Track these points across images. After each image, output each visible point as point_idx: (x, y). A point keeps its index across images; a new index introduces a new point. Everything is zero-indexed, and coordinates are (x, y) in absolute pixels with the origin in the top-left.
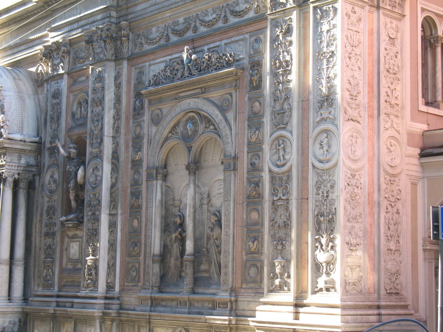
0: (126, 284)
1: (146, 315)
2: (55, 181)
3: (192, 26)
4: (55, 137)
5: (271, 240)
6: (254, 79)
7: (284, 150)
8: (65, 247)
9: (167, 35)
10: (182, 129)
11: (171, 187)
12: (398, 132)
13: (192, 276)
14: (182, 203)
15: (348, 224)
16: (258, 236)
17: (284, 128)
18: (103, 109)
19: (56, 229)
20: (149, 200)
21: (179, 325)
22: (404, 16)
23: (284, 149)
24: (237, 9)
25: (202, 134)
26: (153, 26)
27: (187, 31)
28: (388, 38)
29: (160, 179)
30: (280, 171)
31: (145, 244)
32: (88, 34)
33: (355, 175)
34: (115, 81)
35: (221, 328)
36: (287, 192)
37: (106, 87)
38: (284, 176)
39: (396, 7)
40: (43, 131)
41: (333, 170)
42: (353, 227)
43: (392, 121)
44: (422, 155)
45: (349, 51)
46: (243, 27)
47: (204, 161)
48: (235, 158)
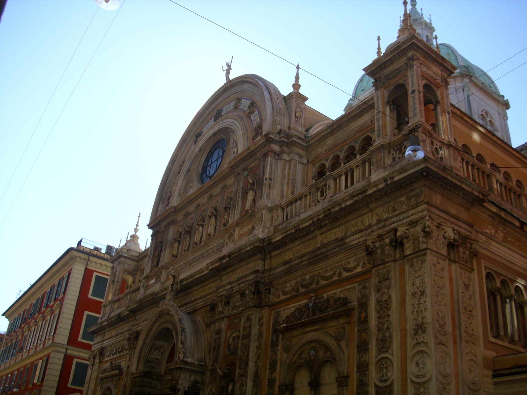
3: (316, 280)
9: (297, 288)
12: (476, 356)
17: (386, 352)
18: (249, 341)
22: (474, 270)
23: (386, 368)
24: (349, 266)
28: (464, 285)
33: (446, 389)
37: (253, 326)
39: (467, 263)
41: (427, 384)
43: (471, 348)
44: (494, 376)
48: (347, 377)
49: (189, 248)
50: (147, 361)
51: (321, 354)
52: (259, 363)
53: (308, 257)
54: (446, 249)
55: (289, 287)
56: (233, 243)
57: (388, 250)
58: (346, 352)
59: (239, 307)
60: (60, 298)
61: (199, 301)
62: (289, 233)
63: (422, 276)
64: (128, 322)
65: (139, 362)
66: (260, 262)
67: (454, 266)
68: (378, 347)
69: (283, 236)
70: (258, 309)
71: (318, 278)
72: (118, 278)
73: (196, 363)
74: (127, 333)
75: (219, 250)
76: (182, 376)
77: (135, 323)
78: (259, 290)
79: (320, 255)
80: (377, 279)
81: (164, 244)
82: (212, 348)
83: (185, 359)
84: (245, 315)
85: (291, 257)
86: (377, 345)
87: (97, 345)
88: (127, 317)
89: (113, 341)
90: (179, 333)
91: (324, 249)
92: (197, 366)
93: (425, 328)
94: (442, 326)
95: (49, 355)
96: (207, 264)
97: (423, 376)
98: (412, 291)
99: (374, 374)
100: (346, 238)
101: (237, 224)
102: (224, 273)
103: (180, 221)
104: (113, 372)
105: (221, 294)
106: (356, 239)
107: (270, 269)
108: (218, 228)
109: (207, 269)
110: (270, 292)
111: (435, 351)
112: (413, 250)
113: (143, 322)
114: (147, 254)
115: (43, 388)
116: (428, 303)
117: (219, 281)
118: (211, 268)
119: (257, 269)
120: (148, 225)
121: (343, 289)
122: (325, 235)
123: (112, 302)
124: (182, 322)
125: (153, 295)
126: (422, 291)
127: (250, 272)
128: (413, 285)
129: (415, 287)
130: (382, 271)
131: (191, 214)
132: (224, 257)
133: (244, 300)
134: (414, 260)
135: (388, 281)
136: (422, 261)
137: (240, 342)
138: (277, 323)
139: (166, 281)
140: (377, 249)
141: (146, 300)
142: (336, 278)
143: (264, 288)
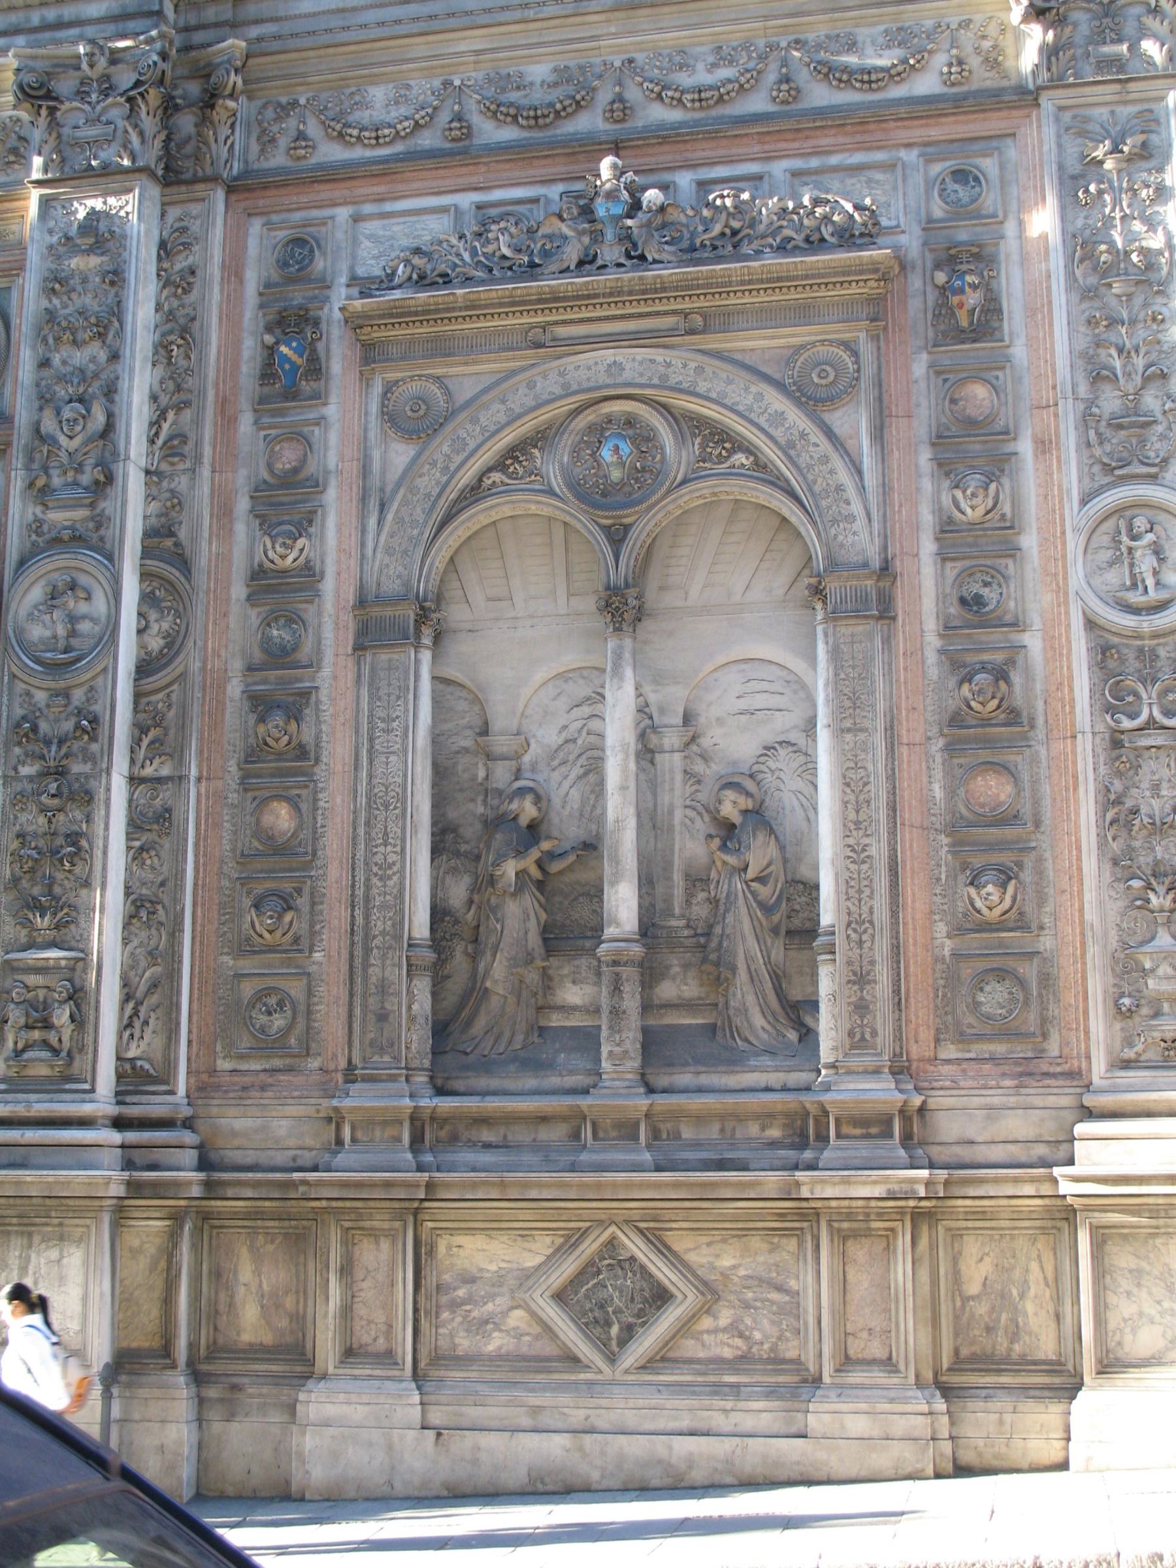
0: (224, 1065)
1: (417, 1186)
5: (1113, 874)
6: (961, 305)
7: (1156, 553)
10: (565, 459)
11: (468, 683)
14: (533, 745)
16: (1020, 865)
17: (1153, 478)
18: (115, 357)
20: (381, 725)
21: (603, 1217)
25: (684, 482)
26: (374, 80)
27: (575, 112)
29: (427, 648)
30: (1145, 624)
32: (31, 63)
34: (159, 259)
35: (868, 1215)
38: (1165, 645)
46: (892, 124)
47: (662, 588)
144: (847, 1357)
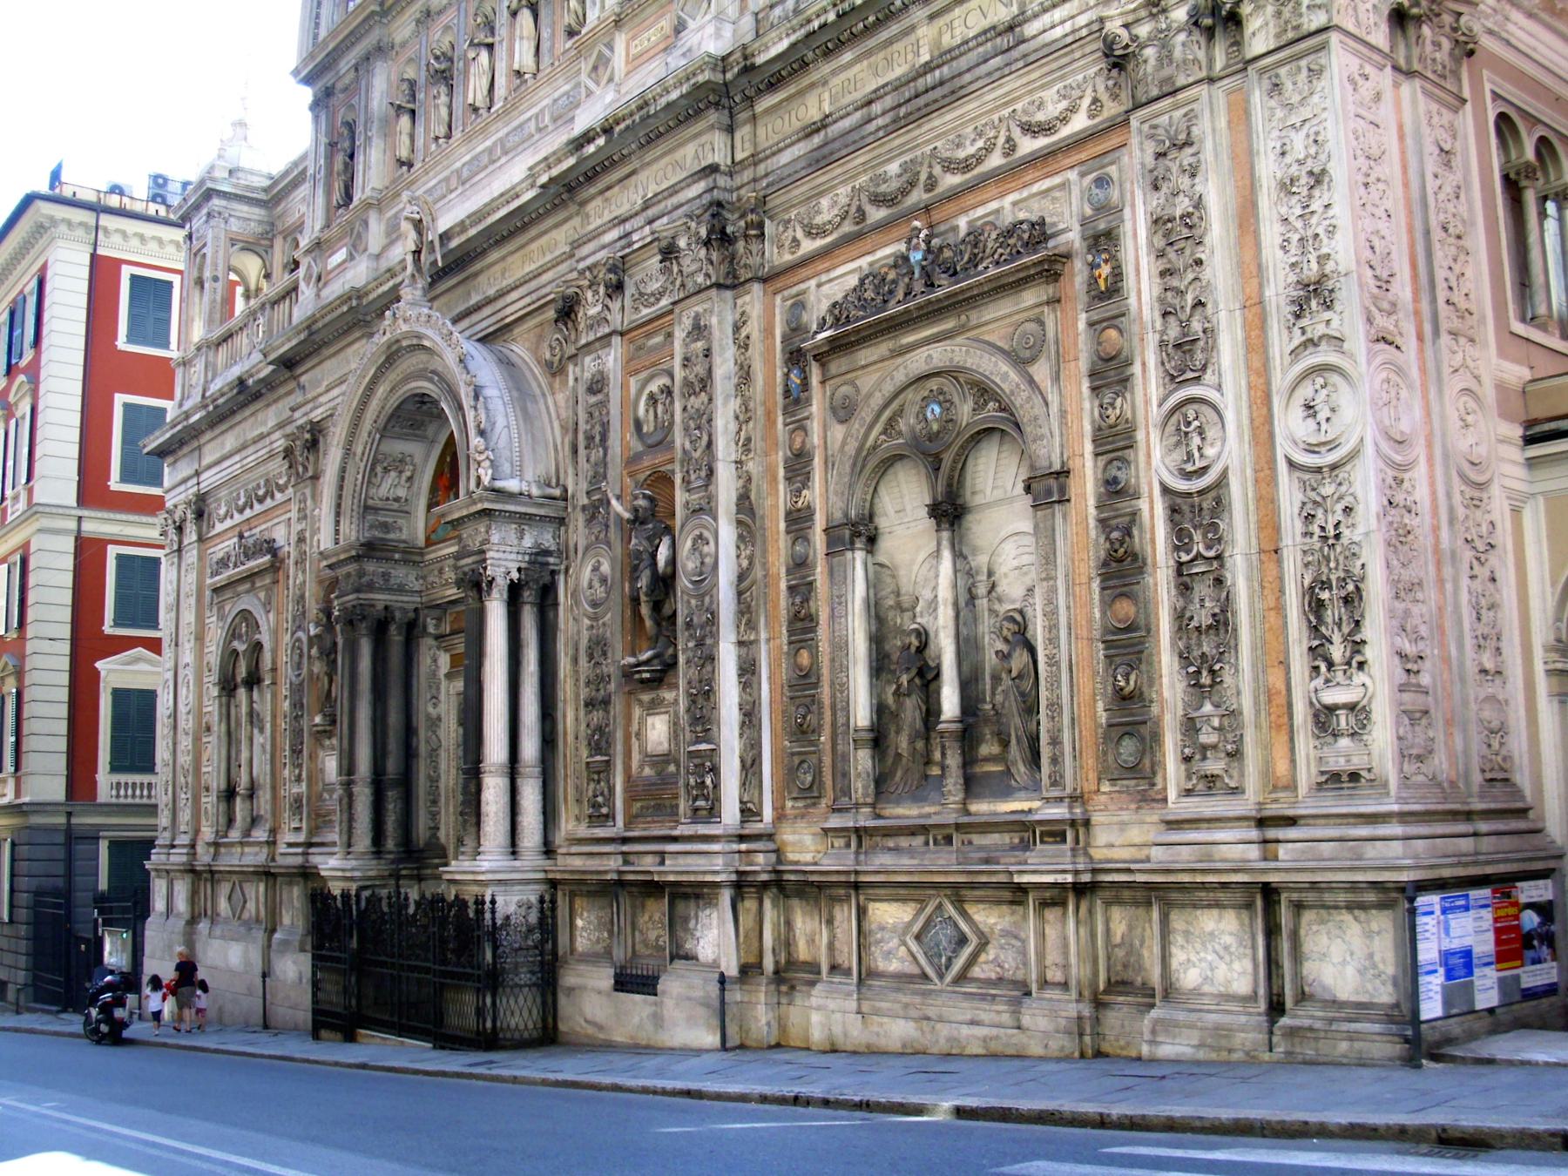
2: (603, 580)
3: (923, 177)
4: (599, 475)
8: (635, 727)
9: (860, 209)
12: (1477, 378)
13: (960, 772)
15: (1397, 604)
18: (710, 400)
19: (612, 687)
22: (1464, 101)
23: (1201, 431)
24: (1040, 117)
28: (1437, 151)
31: (833, 707)
36: (1215, 537)
40: (570, 471)
41: (1348, 467)
42: (1407, 613)
44: (1529, 440)
45: (1364, 169)
47: (974, 493)
48: (1064, 473)
49: (450, 127)
50: (367, 508)
51: (965, 411)
52: (750, 466)
53: (889, 101)
54: (1384, 27)
55: (826, 211)
56: (612, 86)
57: (1184, 44)
58: (1053, 398)
59: (659, 295)
60: (23, 363)
61: (514, 295)
62: (816, 24)
63: (1315, 121)
64: (275, 401)
65: (338, 514)
66: (719, 139)
67: (1408, 89)
68: (1168, 366)
69: (793, 38)
70: (728, 294)
71: (930, 166)
72: (215, 265)
73: (535, 491)
74: (277, 435)
75: (562, 117)
76: (495, 537)
77: (300, 399)
78: (723, 231)
79: (933, 88)
80: (1151, 148)
81: (360, 129)
82: (581, 437)
83: (499, 484)
84: (684, 319)
85: (827, 109)
86: (1163, 364)
87: (182, 488)
88: (269, 384)
89: (233, 466)
90: (467, 402)
91: (945, 69)
92: (541, 500)
93: (1332, 291)
94: (1384, 284)
95: (26, 546)
96: (530, 169)
97: (1332, 445)
98: (1279, 175)
99: (1157, 453)
100: (1026, 21)
101: (618, 23)
102: (593, 190)
103: (403, 45)
104: (252, 564)
105: (589, 262)
106: (1063, 22)
107: (755, 159)
108: (545, 46)
109: (532, 186)
110: (763, 234)
111: (1369, 363)
112: (1278, 36)
113: (327, 391)
114: (304, 170)
115: (30, 647)
116: (1341, 212)
117: (576, 221)
118: (544, 179)
119: (709, 161)
120: (296, 72)
121: (1025, 193)
122: (947, 18)
123: (209, 347)
124: (471, 365)
125: (350, 298)
126: (1317, 170)
127: (685, 174)
128: (1283, 154)
129: (1288, 159)
130: (1166, 117)
131: (440, 13)
132: (587, 137)
133: (675, 269)
134: (1283, 71)
135: (1188, 151)
136: (1310, 70)
137: (678, 407)
138: (795, 330)
139: (385, 248)
140: (1142, 47)
141: (328, 318)
142: (996, 160)
143: (742, 223)
144: (1303, 992)
